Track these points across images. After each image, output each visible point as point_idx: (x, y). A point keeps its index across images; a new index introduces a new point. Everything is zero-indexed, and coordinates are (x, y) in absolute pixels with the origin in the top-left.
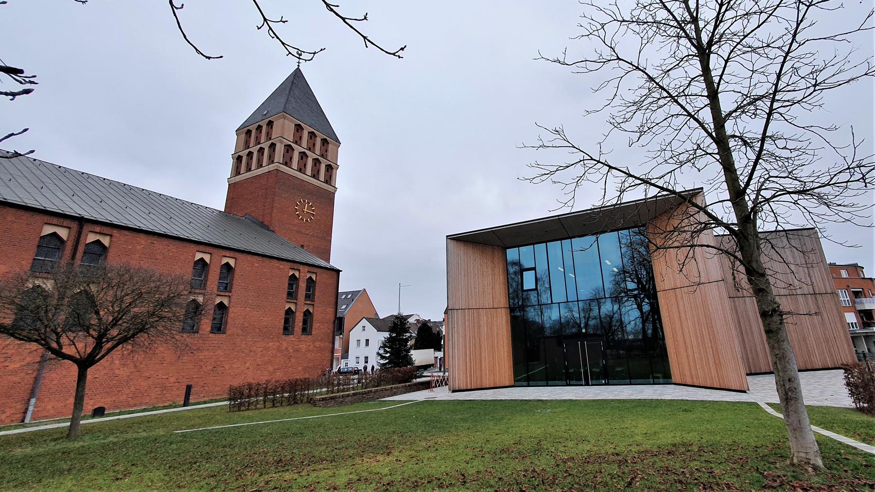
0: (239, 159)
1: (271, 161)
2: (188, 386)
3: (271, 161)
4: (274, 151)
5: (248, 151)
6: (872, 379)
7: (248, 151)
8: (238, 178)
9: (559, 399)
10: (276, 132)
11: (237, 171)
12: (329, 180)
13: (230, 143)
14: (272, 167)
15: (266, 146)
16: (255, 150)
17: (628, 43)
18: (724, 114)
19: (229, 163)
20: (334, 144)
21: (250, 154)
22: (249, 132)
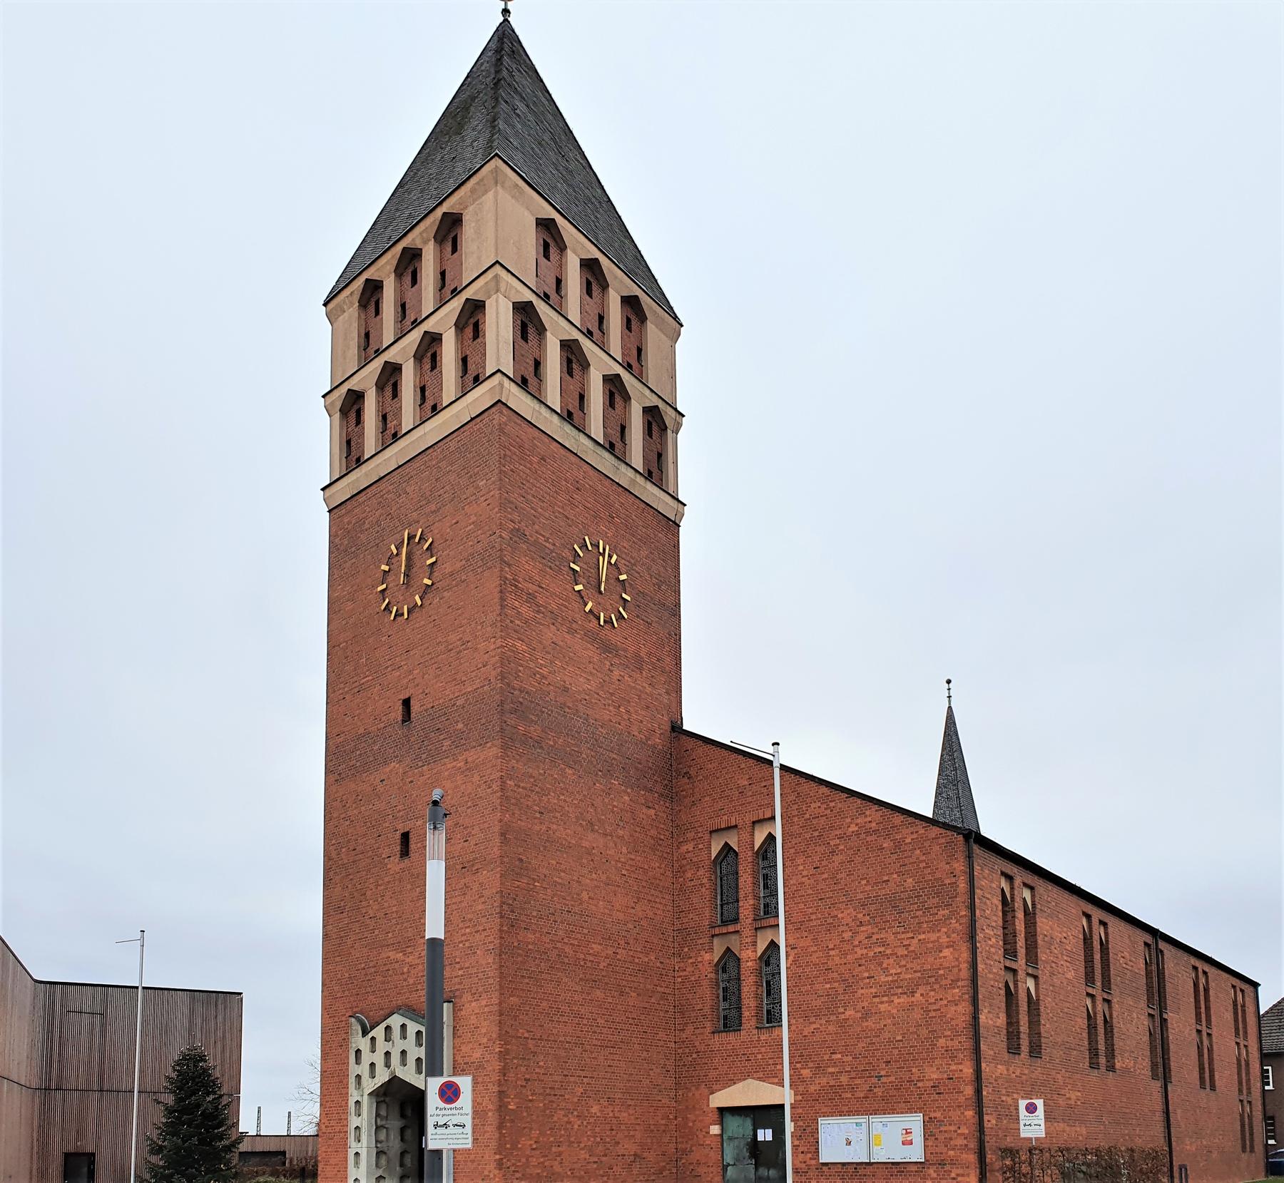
0: (350, 407)
1: (471, 376)
2: (405, 1038)
3: (471, 376)
4: (477, 332)
5: (377, 365)
6: (225, 1179)
7: (377, 365)
8: (362, 477)
9: (61, 1169)
10: (477, 246)
11: (350, 454)
12: (658, 467)
13: (309, 354)
14: (480, 397)
15: (444, 321)
16: (403, 351)
17: (162, 1098)
18: (920, 798)
19: (319, 431)
20: (660, 325)
21: (390, 377)
22: (373, 288)
